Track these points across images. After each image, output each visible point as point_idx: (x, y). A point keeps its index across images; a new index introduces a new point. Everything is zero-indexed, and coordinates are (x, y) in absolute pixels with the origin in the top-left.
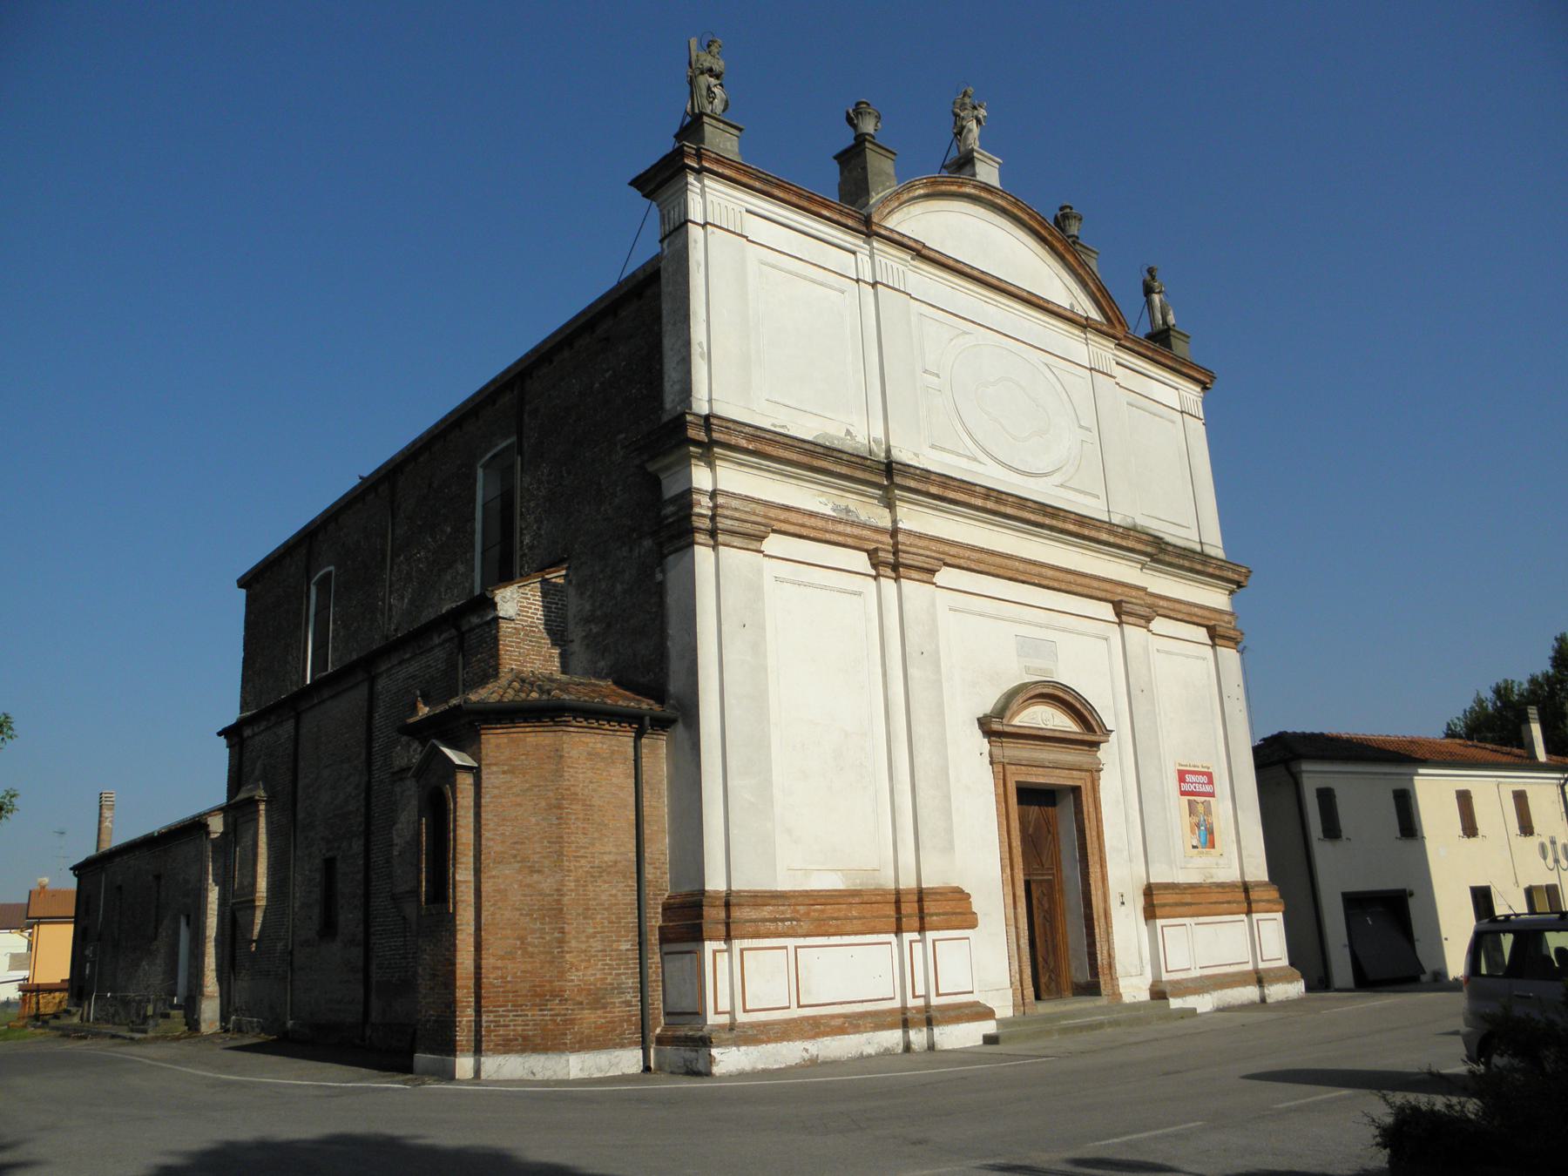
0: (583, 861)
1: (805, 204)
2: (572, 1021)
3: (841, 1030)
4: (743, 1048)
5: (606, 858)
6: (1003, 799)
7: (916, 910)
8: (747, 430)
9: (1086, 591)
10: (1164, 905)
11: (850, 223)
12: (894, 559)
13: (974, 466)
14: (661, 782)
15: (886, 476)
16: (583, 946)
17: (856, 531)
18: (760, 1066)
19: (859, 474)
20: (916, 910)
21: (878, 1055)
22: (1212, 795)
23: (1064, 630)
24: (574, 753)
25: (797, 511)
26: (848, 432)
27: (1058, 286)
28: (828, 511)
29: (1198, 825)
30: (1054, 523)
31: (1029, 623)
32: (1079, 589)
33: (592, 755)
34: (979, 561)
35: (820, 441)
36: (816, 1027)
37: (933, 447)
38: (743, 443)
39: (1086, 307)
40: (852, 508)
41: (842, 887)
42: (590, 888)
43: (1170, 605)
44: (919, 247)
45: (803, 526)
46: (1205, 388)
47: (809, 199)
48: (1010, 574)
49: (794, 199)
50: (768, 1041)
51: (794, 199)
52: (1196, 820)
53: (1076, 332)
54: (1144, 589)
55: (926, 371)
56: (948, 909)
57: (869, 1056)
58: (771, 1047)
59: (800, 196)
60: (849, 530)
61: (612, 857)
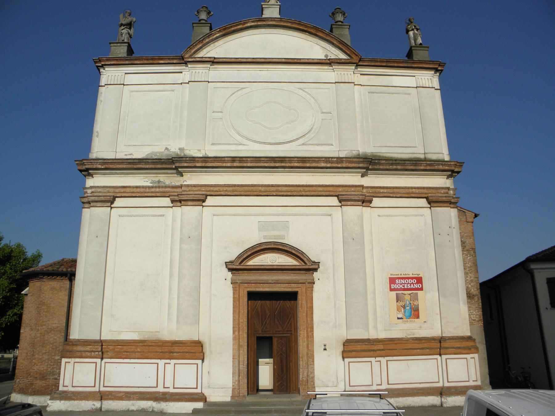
0: (44, 327)
1: (151, 62)
2: (32, 384)
3: (121, 399)
4: (62, 402)
5: (54, 325)
6: (236, 300)
7: (194, 350)
8: (100, 161)
9: (312, 193)
10: (447, 348)
11: (175, 61)
12: (180, 199)
13: (240, 147)
14: (263, 287)
15: (175, 163)
16: (40, 357)
17: (161, 190)
18: (70, 409)
19: (159, 166)
20: (194, 350)
21: (137, 411)
22: (421, 289)
23: (295, 215)
24: (45, 288)
25: (130, 187)
26: (167, 149)
27: (316, 48)
28: (148, 184)
29: (404, 307)
30: (283, 164)
31: (269, 215)
32: (308, 193)
33: (53, 289)
34: (233, 191)
35: (149, 157)
36: (102, 396)
37: (213, 144)
38: (100, 166)
39: (336, 54)
40: (162, 180)
41: (137, 338)
42: (46, 336)
43: (391, 191)
44: (212, 60)
45: (132, 193)
46: (436, 70)
47: (152, 59)
48: (255, 193)
49: (146, 62)
50: (77, 399)
51: (146, 62)
52: (401, 303)
53: (326, 67)
54: (362, 186)
55: (214, 112)
56: (186, 350)
57: (133, 411)
58: (76, 402)
59: (148, 60)
60: (158, 190)
61: (56, 325)
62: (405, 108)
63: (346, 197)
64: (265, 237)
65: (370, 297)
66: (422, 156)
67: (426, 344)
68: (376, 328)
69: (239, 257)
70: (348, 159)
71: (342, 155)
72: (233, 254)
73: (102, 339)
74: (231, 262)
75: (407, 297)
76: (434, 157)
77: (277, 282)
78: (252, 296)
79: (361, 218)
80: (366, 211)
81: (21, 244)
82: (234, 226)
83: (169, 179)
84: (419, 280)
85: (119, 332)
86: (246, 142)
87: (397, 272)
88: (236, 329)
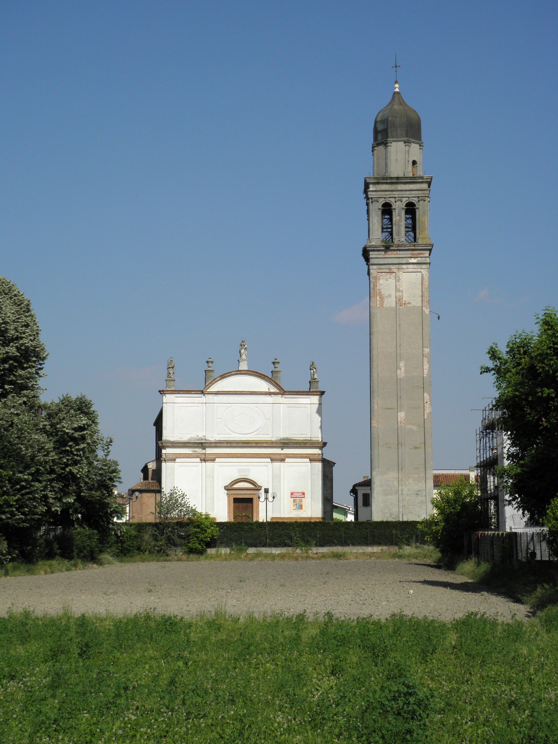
6: (229, 501)
13: (229, 436)
15: (202, 444)
39: (273, 389)
62: (300, 416)
63: (274, 459)
64: (240, 475)
65: (282, 500)
66: (309, 439)
67: (492, 484)
68: (284, 513)
69: (230, 484)
70: (276, 442)
71: (274, 439)
72: (227, 483)
73: (155, 458)
74: (227, 486)
75: (298, 501)
76: (315, 439)
77: (245, 494)
78: (236, 500)
79: (280, 468)
80: (282, 464)
81: (88, 398)
82: (227, 470)
83: (200, 451)
84: (304, 494)
85: (165, 429)
86: (232, 433)
87: (294, 491)
88: (229, 512)
